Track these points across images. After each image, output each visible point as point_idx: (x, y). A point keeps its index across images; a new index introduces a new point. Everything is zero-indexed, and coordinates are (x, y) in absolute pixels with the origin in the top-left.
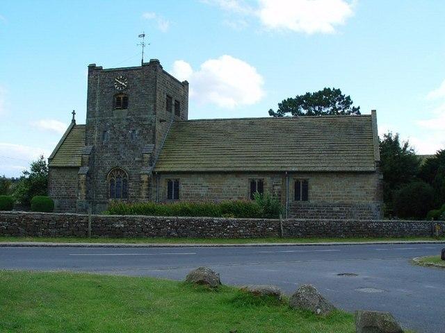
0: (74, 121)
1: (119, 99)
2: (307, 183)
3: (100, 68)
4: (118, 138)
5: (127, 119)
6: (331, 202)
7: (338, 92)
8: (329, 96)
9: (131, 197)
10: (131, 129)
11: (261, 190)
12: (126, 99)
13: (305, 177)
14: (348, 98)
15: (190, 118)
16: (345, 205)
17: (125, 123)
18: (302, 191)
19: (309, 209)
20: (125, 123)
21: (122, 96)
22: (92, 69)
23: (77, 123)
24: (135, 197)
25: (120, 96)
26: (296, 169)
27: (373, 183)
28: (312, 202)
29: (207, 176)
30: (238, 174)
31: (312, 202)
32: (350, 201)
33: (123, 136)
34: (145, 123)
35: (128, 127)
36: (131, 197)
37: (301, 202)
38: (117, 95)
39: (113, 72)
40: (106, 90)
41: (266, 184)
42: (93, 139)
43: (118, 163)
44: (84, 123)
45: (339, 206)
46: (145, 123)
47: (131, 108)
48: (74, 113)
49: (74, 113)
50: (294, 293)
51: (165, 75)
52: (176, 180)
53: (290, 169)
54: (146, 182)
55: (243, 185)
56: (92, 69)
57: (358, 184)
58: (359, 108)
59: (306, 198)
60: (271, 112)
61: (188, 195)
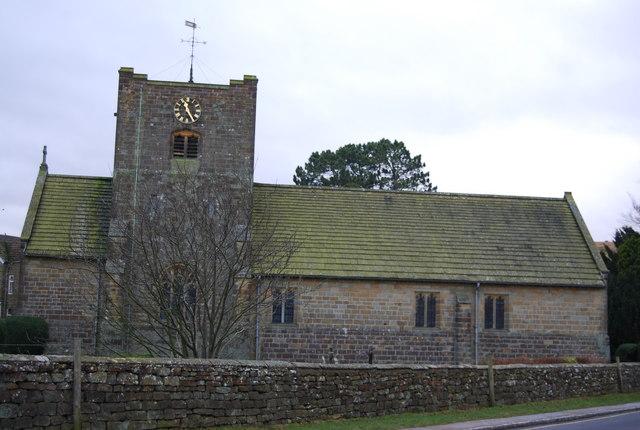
1: (180, 138)
2: (503, 301)
3: (143, 78)
6: (540, 330)
7: (399, 145)
11: (277, 309)
12: (193, 140)
13: (502, 292)
14: (419, 158)
15: (258, 178)
16: (561, 336)
18: (496, 314)
21: (186, 134)
22: (126, 76)
23: (51, 172)
25: (183, 134)
26: (492, 279)
27: (599, 302)
28: (513, 330)
29: (346, 285)
30: (397, 282)
31: (513, 330)
32: (567, 331)
34: (233, 186)
37: (495, 331)
38: (178, 130)
39: (172, 90)
41: (443, 302)
45: (551, 337)
46: (233, 186)
47: (206, 154)
49: (45, 153)
52: (432, 294)
53: (482, 279)
54: (246, 292)
55: (404, 302)
56: (126, 76)
57: (579, 305)
58: (428, 174)
59: (501, 325)
60: (435, 188)
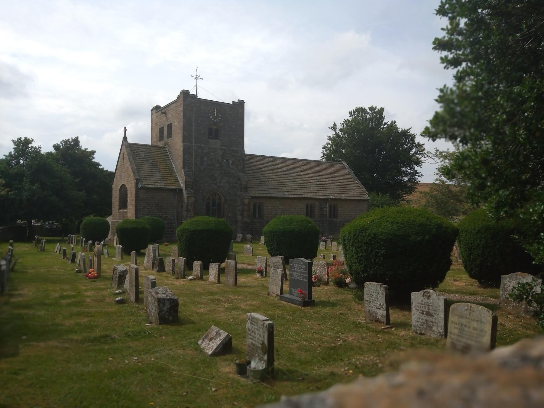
0: (125, 139)
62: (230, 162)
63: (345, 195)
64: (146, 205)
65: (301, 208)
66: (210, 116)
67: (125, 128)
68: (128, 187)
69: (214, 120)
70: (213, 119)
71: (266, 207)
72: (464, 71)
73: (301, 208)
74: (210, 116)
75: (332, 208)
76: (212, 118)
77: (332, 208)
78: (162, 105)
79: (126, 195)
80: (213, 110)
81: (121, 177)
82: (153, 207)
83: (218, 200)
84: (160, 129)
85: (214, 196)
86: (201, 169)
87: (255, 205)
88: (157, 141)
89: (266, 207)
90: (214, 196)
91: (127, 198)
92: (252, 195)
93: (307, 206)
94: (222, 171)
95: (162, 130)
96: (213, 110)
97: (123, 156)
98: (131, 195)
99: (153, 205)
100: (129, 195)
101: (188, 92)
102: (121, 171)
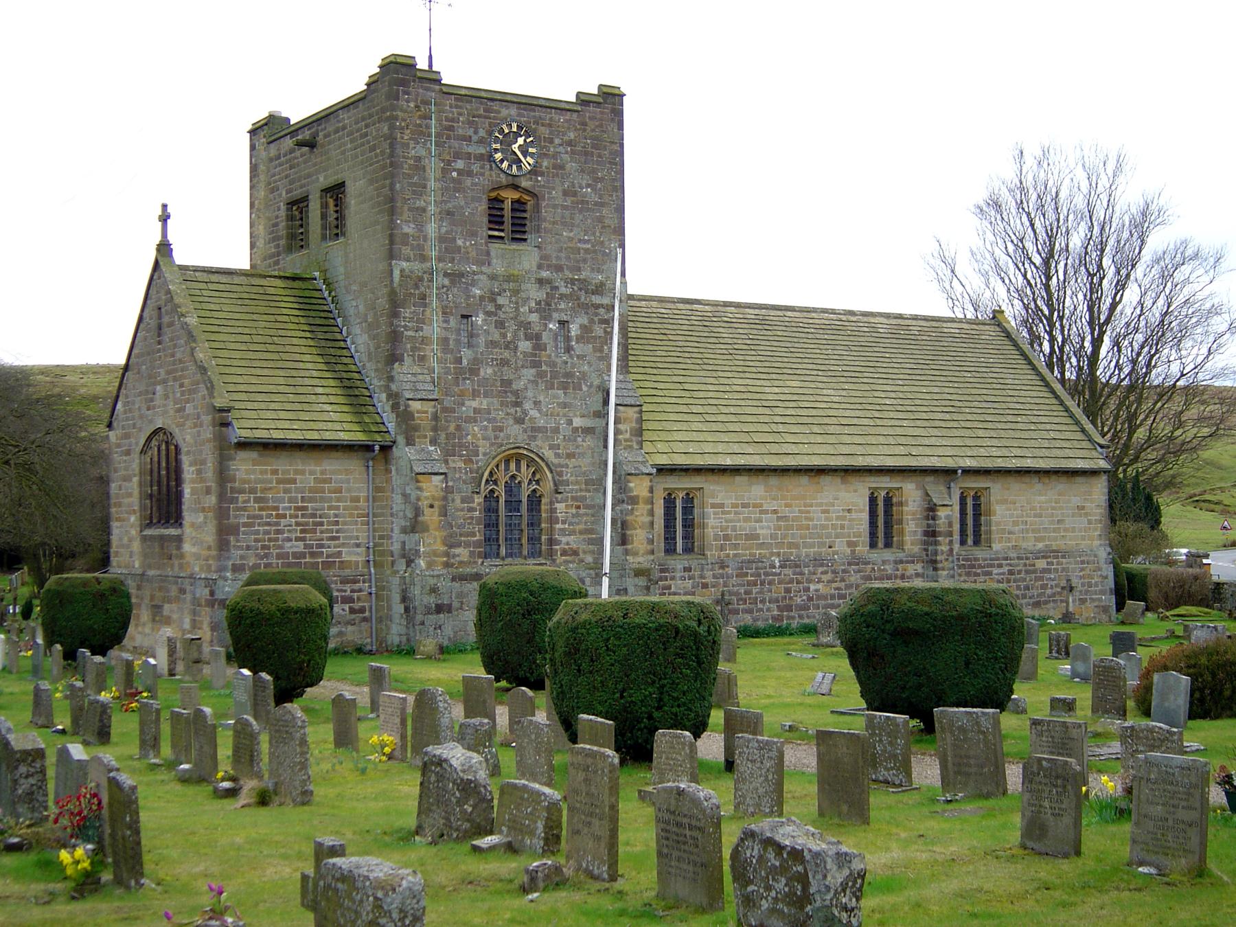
0: (164, 248)
4: (511, 346)
5: (541, 282)
6: (1028, 545)
8: (253, 132)
9: (564, 553)
10: (555, 315)
17: (536, 294)
19: (992, 566)
20: (536, 294)
21: (510, 195)
24: (575, 553)
29: (774, 481)
31: (996, 546)
33: (527, 338)
35: (545, 309)
36: (564, 553)
40: (460, 164)
42: (425, 341)
43: (515, 433)
44: (238, 257)
48: (164, 218)
49: (164, 218)
50: (263, 811)
51: (547, 116)
61: (726, 537)
62: (574, 330)
63: (1018, 452)
64: (261, 509)
65: (849, 511)
66: (496, 150)
67: (165, 206)
68: (186, 438)
69: (510, 166)
70: (505, 164)
71: (713, 506)
72: (1127, 494)
73: (849, 511)
74: (496, 150)
75: (970, 502)
76: (502, 161)
77: (970, 502)
78: (296, 113)
79: (176, 474)
80: (504, 127)
81: (152, 400)
82: (284, 516)
83: (530, 482)
84: (291, 204)
85: (513, 466)
86: (465, 362)
87: (669, 503)
88: (279, 254)
89: (713, 506)
90: (513, 466)
91: (179, 481)
92: (663, 460)
93: (873, 501)
94: (544, 368)
95: (298, 205)
96: (504, 127)
97: (160, 317)
98: (199, 472)
99: (285, 508)
100: (189, 472)
101: (410, 61)
102: (150, 377)
